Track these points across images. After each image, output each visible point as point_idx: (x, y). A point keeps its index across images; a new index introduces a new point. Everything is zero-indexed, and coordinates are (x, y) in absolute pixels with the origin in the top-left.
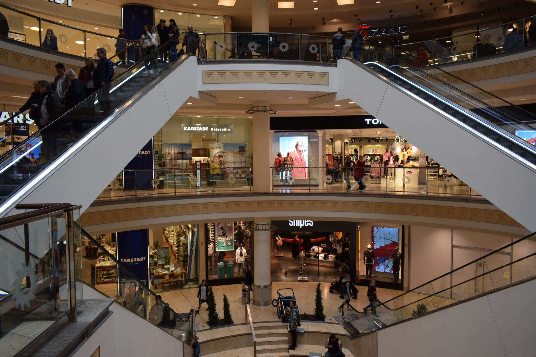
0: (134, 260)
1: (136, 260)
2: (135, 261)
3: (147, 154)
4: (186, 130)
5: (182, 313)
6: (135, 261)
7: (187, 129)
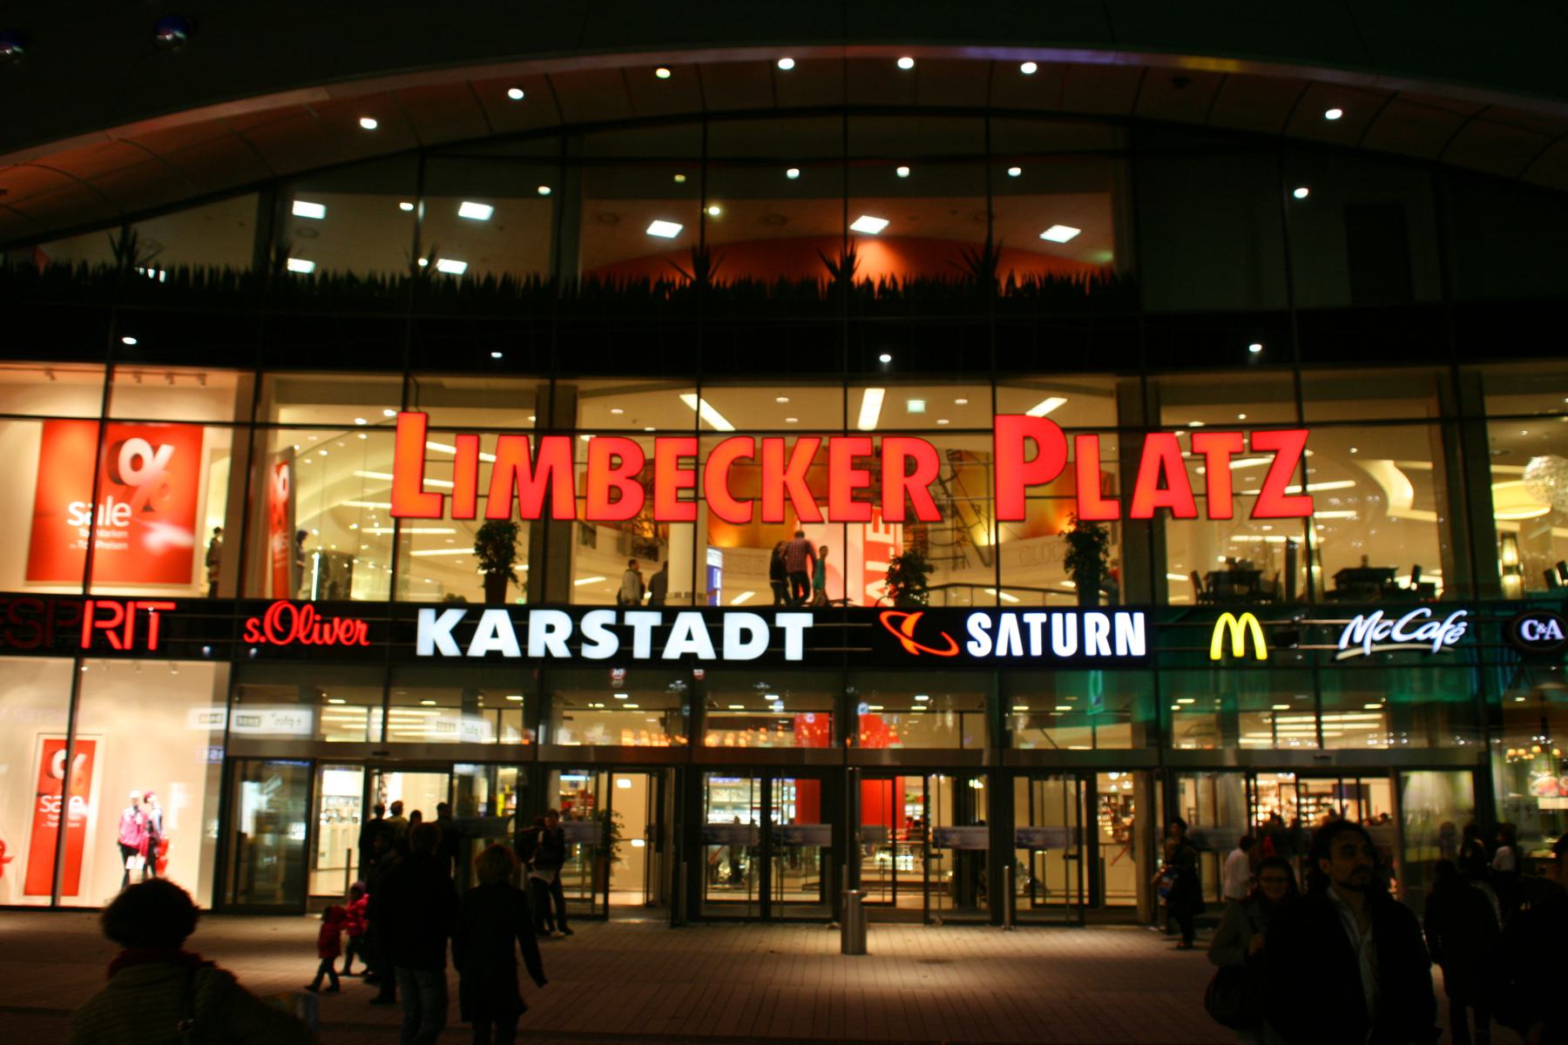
0: (625, 634)
1: (660, 636)
2: (642, 649)
3: (758, 647)
4: (450, 648)
6: (642, 649)
7: (463, 633)
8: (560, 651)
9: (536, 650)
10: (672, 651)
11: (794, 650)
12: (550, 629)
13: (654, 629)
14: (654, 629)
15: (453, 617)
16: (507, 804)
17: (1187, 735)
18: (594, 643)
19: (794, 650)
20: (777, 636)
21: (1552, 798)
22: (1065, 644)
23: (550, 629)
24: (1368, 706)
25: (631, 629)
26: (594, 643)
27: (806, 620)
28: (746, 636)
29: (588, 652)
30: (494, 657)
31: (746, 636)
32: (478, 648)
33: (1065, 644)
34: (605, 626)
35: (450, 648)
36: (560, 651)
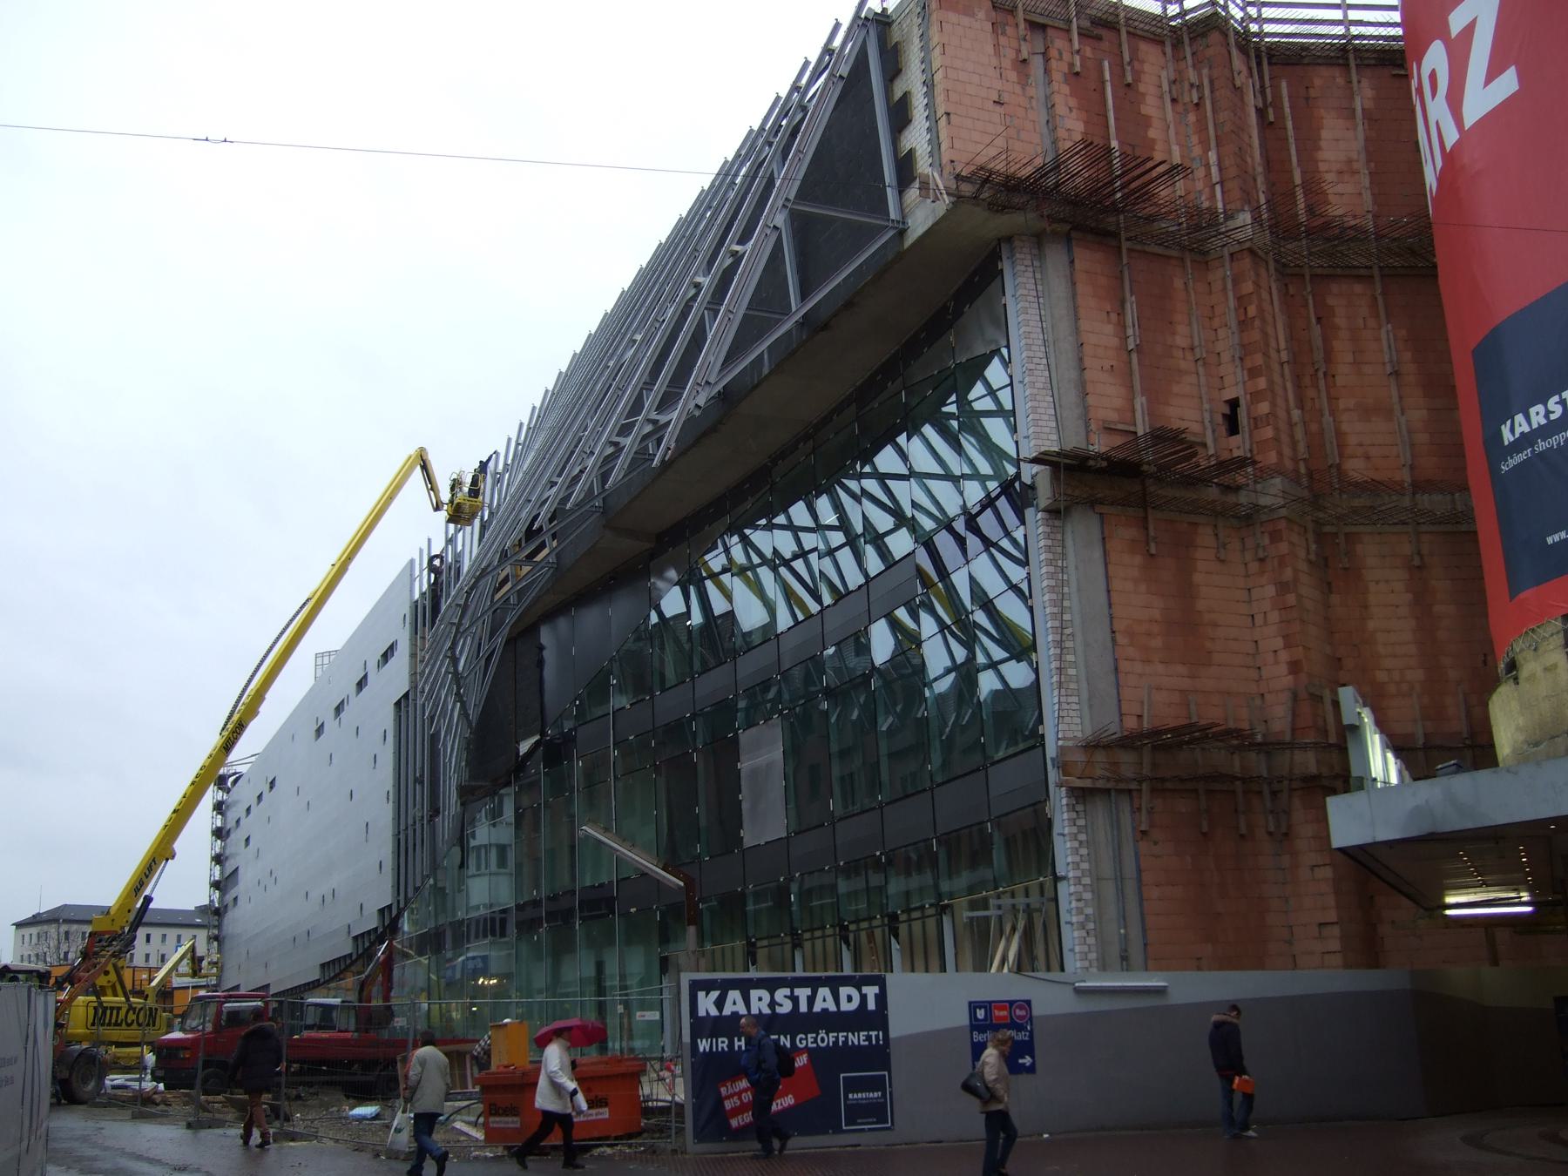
0: (795, 1000)
1: (811, 1000)
2: (803, 1008)
3: (854, 1005)
4: (714, 1012)
5: (1043, 735)
6: (803, 1008)
7: (720, 1003)
8: (767, 1011)
10: (817, 1008)
12: (760, 999)
13: (808, 997)
14: (808, 997)
15: (715, 994)
16: (788, 1045)
17: (671, 1089)
18: (781, 1005)
20: (864, 998)
21: (1141, 798)
22: (429, 540)
23: (760, 999)
24: (859, 1121)
25: (797, 997)
26: (781, 1005)
28: (850, 999)
29: (779, 1010)
30: (825, 1011)
31: (850, 999)
32: (727, 1011)
33: (429, 540)
34: (786, 997)
35: (714, 1012)
36: (767, 1011)
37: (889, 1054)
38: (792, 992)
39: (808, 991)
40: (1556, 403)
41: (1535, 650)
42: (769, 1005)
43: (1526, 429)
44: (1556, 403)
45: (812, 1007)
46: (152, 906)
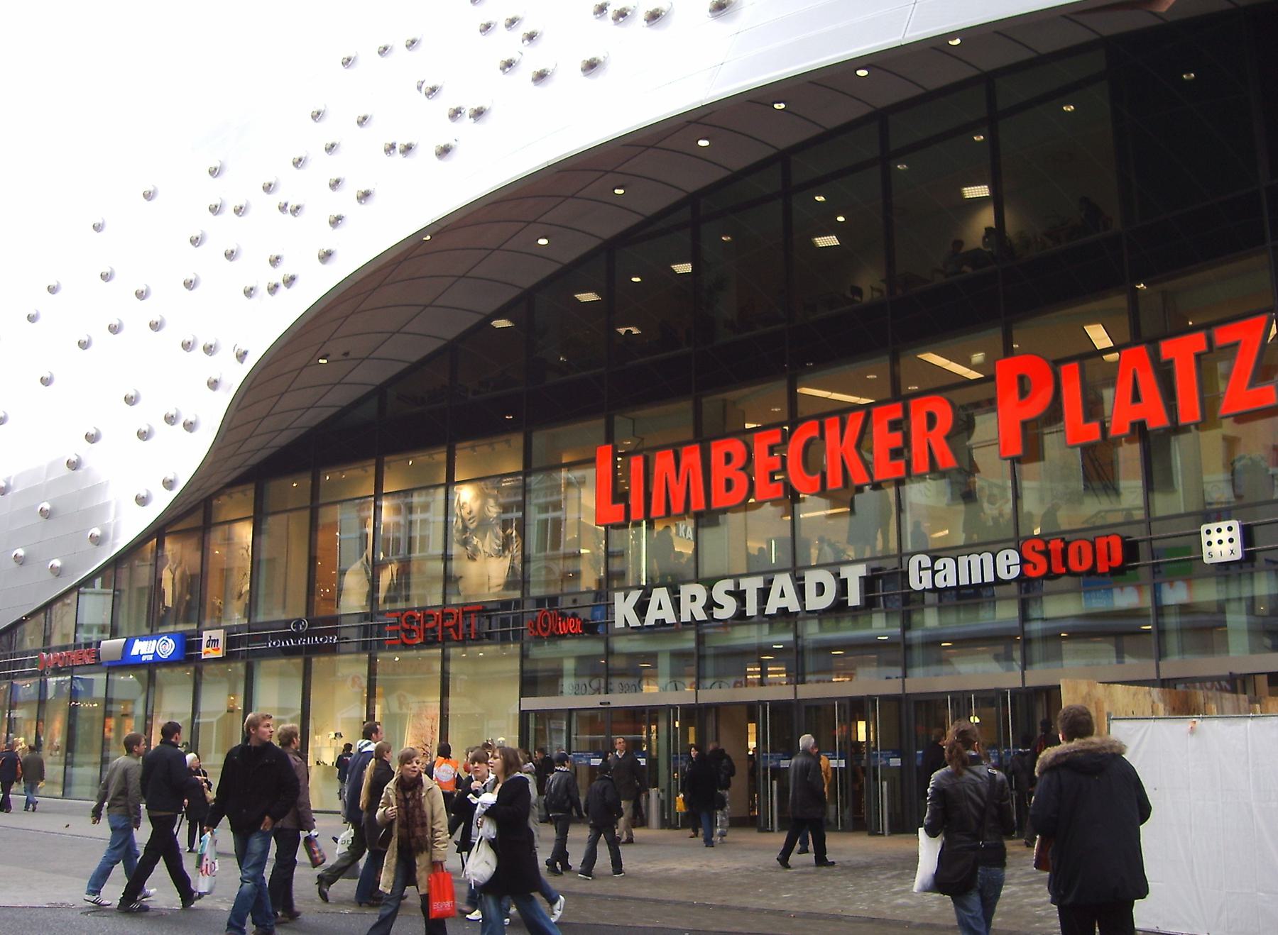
0: (739, 595)
1: (764, 594)
2: (752, 609)
4: (634, 621)
6: (752, 609)
7: (641, 608)
8: (701, 616)
9: (686, 617)
11: (854, 598)
19: (854, 598)
20: (843, 585)
23: (694, 598)
27: (862, 570)
28: (821, 588)
29: (718, 614)
30: (661, 623)
31: (821, 588)
35: (634, 621)
36: (701, 616)
37: (967, 34)
38: (737, 585)
39: (758, 582)
40: (728, 593)
41: (21, 564)
42: (253, 923)
43: (668, 615)
44: (728, 593)
45: (428, 917)
46: (1017, 391)
